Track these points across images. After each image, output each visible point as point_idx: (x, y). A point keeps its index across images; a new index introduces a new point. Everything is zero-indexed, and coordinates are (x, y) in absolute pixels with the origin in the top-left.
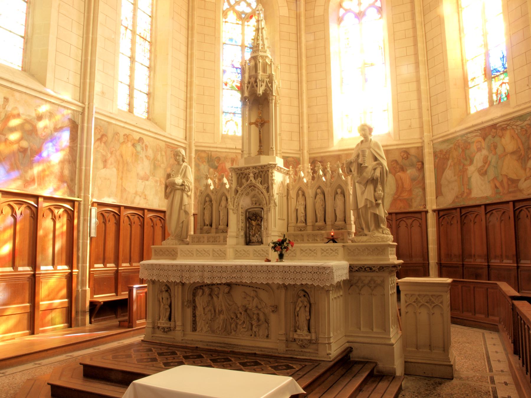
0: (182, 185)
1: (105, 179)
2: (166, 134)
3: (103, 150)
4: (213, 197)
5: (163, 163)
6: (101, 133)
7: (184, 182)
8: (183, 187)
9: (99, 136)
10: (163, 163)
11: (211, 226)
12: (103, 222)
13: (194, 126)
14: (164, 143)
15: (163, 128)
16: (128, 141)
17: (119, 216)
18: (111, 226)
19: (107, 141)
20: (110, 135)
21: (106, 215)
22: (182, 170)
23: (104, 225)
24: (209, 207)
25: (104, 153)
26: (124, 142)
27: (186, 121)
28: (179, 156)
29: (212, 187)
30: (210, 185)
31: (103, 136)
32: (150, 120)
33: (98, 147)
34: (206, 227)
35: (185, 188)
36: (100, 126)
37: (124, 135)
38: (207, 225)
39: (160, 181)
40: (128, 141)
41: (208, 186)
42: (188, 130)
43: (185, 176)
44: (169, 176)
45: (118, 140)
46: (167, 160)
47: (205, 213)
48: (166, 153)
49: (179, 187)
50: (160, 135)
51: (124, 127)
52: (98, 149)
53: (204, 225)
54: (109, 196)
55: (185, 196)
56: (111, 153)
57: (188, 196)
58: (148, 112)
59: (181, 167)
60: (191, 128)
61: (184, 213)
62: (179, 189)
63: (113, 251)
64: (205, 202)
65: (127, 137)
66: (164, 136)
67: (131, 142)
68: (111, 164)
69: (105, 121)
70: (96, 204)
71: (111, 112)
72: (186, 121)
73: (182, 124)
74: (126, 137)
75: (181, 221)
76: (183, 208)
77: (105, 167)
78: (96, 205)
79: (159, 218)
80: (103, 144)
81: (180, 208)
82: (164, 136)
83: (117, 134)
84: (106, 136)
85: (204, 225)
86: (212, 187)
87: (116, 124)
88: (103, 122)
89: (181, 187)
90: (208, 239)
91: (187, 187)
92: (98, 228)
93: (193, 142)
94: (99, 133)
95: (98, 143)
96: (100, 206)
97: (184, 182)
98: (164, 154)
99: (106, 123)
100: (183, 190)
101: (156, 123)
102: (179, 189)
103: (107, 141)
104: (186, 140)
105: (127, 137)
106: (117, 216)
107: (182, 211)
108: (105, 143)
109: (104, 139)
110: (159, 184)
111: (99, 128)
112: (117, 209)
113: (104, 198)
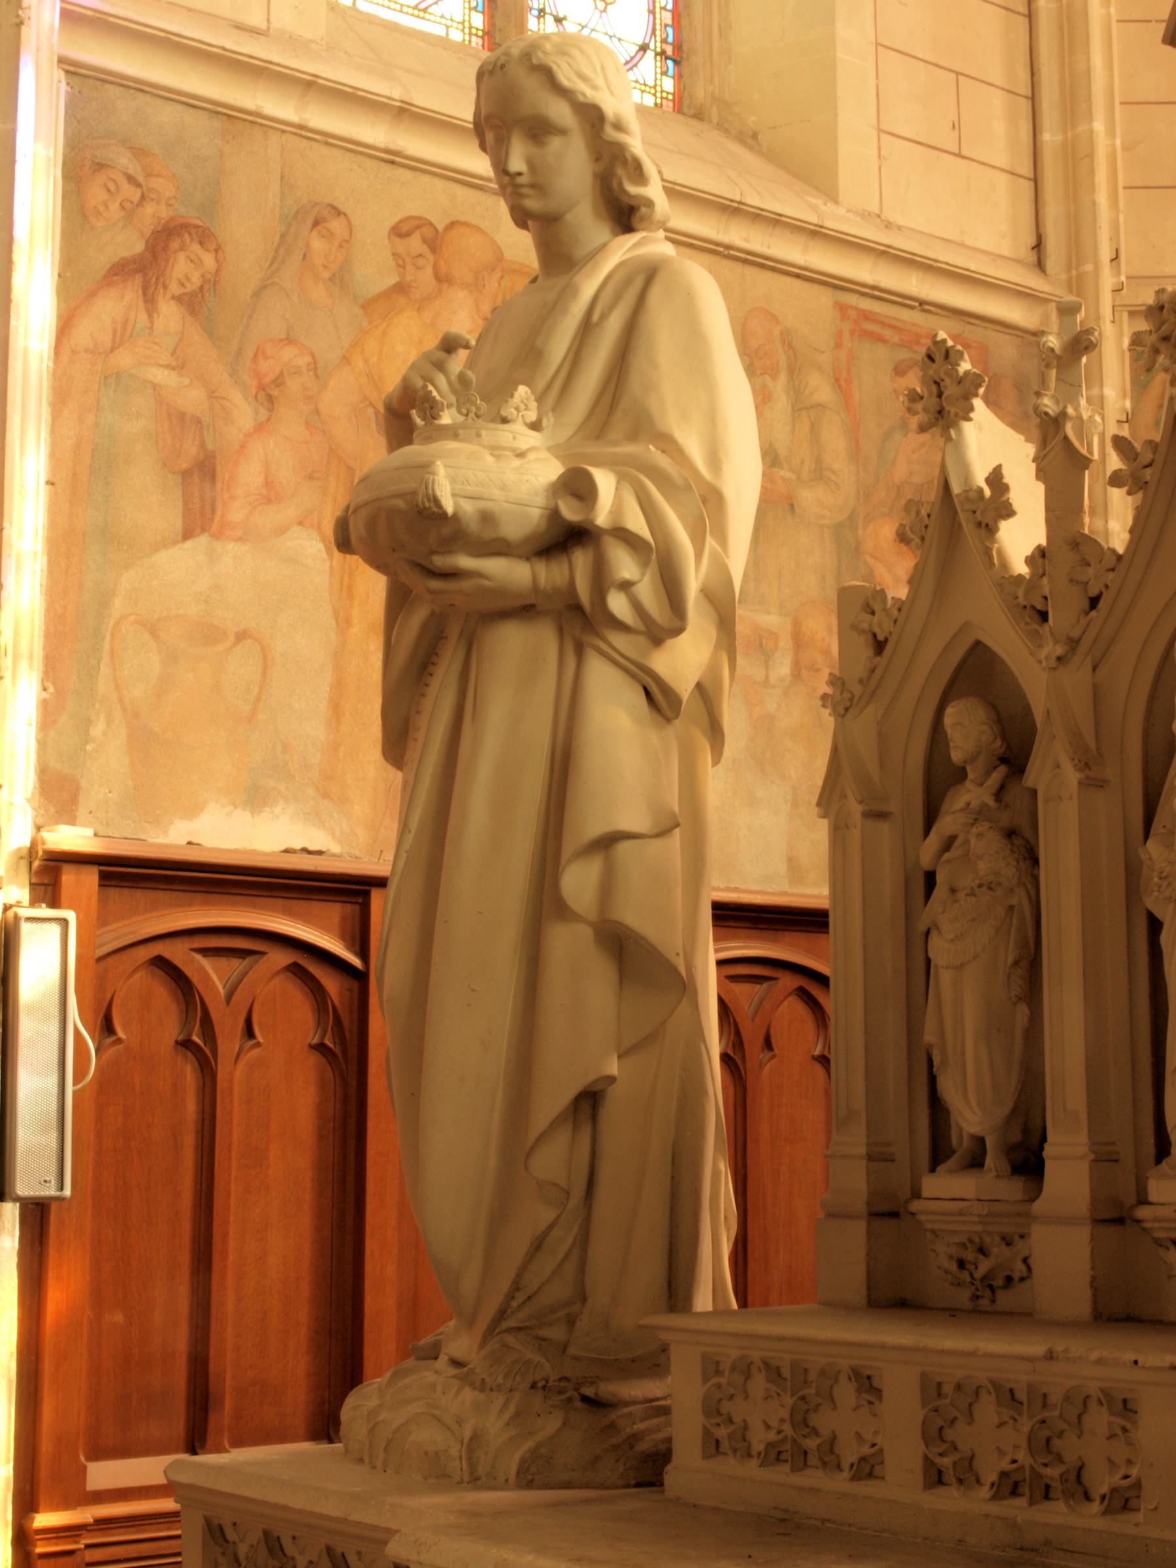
0: (566, 537)
1: (207, 634)
2: (837, 219)
3: (179, 368)
4: (1030, 666)
5: (820, 474)
6: (152, 214)
7: (577, 485)
8: (581, 559)
9: (132, 244)
10: (820, 474)
11: (1028, 1163)
12: (186, 1044)
13: (1102, 131)
14: (825, 299)
15: (818, 176)
16: (443, 279)
17: (360, 977)
18: (275, 1082)
19: (211, 283)
20: (246, 231)
21: (212, 975)
22: (587, 328)
23: (189, 1073)
24: (987, 854)
25: (192, 399)
26: (401, 288)
27: (1034, 98)
28: (539, 130)
29: (1021, 537)
30: (996, 504)
31: (165, 238)
32: (699, 115)
33: (121, 337)
34: (947, 1187)
35: (601, 580)
36: (139, 153)
37: (399, 232)
38: (976, 1162)
39: (799, 641)
40: (443, 279)
41: (956, 521)
42: (1049, 178)
43: (618, 408)
44: (405, 416)
45: (340, 278)
46: (855, 453)
47: (940, 950)
48: (842, 384)
49: (513, 573)
50: (776, 222)
51: (392, 158)
52: (124, 359)
53: (939, 1154)
54: (255, 798)
55: (612, 712)
56: (268, 395)
57: (658, 699)
58: (676, 55)
59: (569, 292)
60: (1077, 156)
61: (600, 975)
62: (524, 610)
63: (303, 1314)
64: (939, 779)
65: (434, 243)
66: (816, 234)
67: (476, 286)
68: (270, 494)
69: (191, 102)
70: (91, 877)
71: (256, 19)
72: (1034, 98)
73: (996, 133)
74: (415, 244)
75: (554, 1096)
76: (579, 882)
77: (199, 521)
78: (82, 883)
79: (789, 981)
80: (169, 314)
81: (545, 903)
82: (816, 234)
83: (323, 216)
84: (204, 236)
85: (939, 1154)
86: (1021, 537)
87: (301, 129)
88: (167, 115)
89: (550, 574)
90: (935, 1433)
91: (625, 565)
92: (105, 1111)
93: (1108, 281)
94: (130, 212)
95: (112, 307)
96: (120, 896)
97: (577, 485)
98: (821, 390)
99: (195, 122)
100: (579, 621)
101: (750, 139)
102: (524, 610)
103: (211, 283)
104: (1040, 265)
105: (434, 243)
106: (332, 983)
107: (568, 944)
108: (193, 303)
109: (185, 268)
110: (783, 667)
111: (125, 161)
112: (335, 911)
113: (193, 811)
